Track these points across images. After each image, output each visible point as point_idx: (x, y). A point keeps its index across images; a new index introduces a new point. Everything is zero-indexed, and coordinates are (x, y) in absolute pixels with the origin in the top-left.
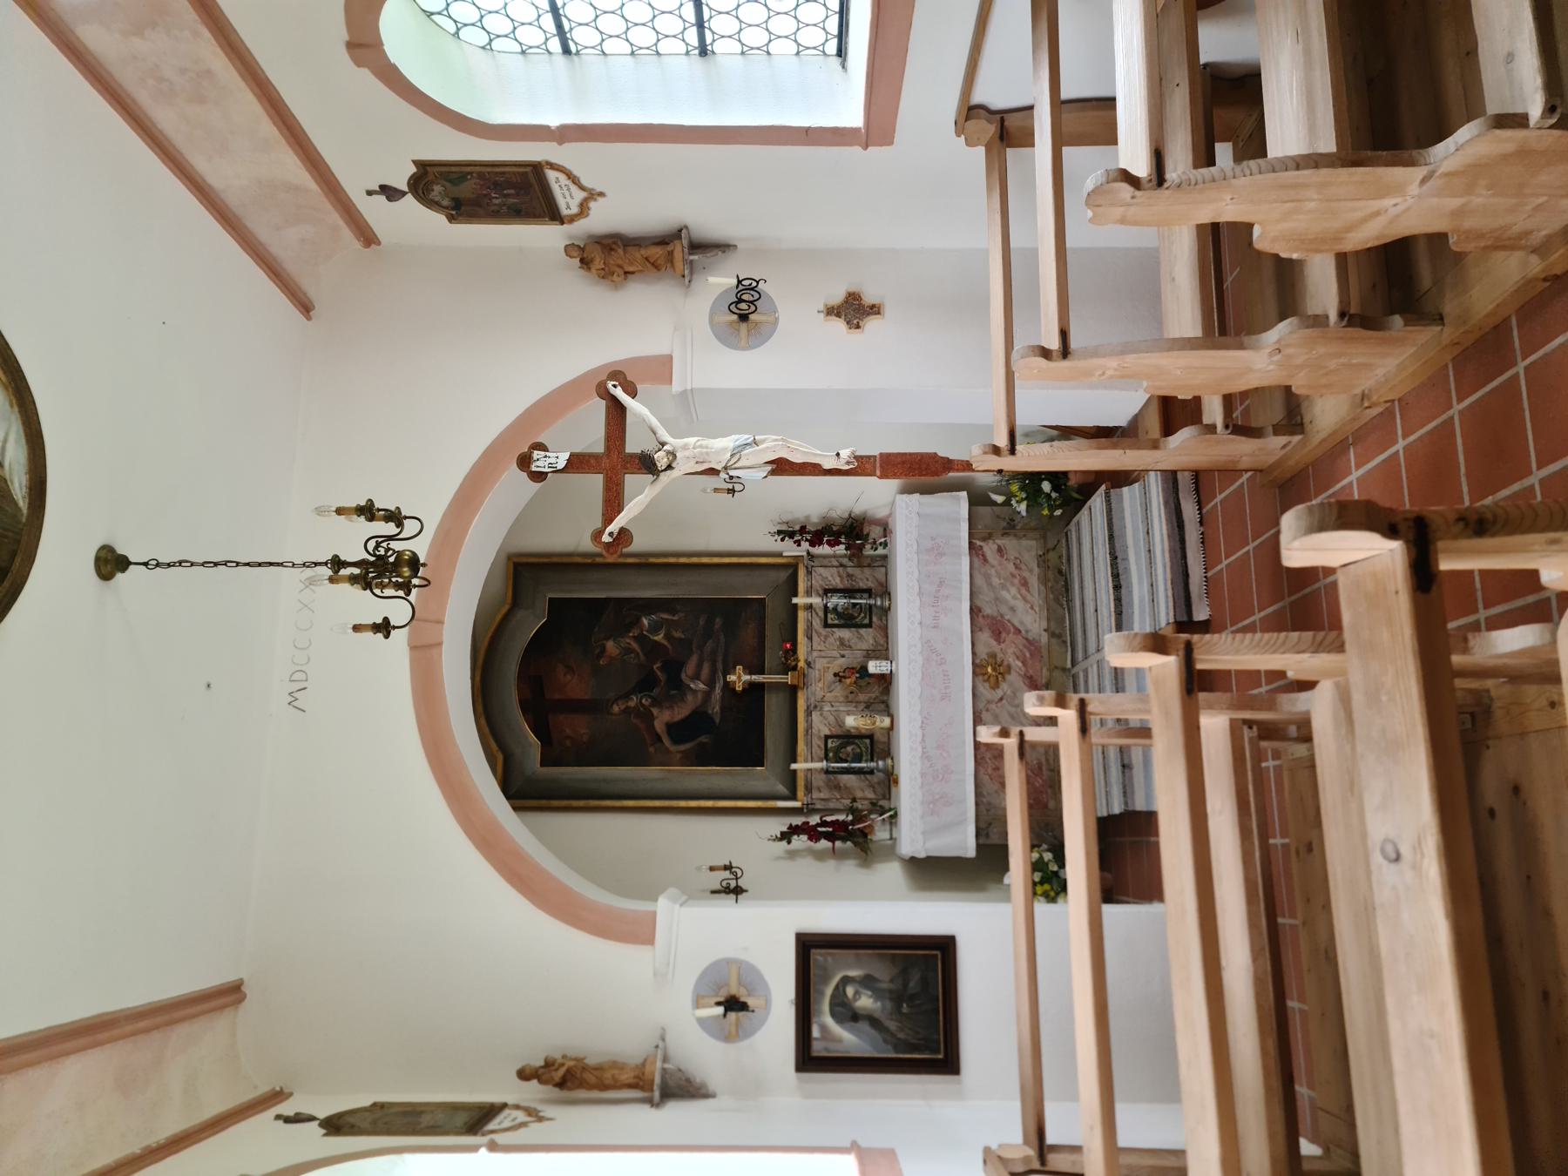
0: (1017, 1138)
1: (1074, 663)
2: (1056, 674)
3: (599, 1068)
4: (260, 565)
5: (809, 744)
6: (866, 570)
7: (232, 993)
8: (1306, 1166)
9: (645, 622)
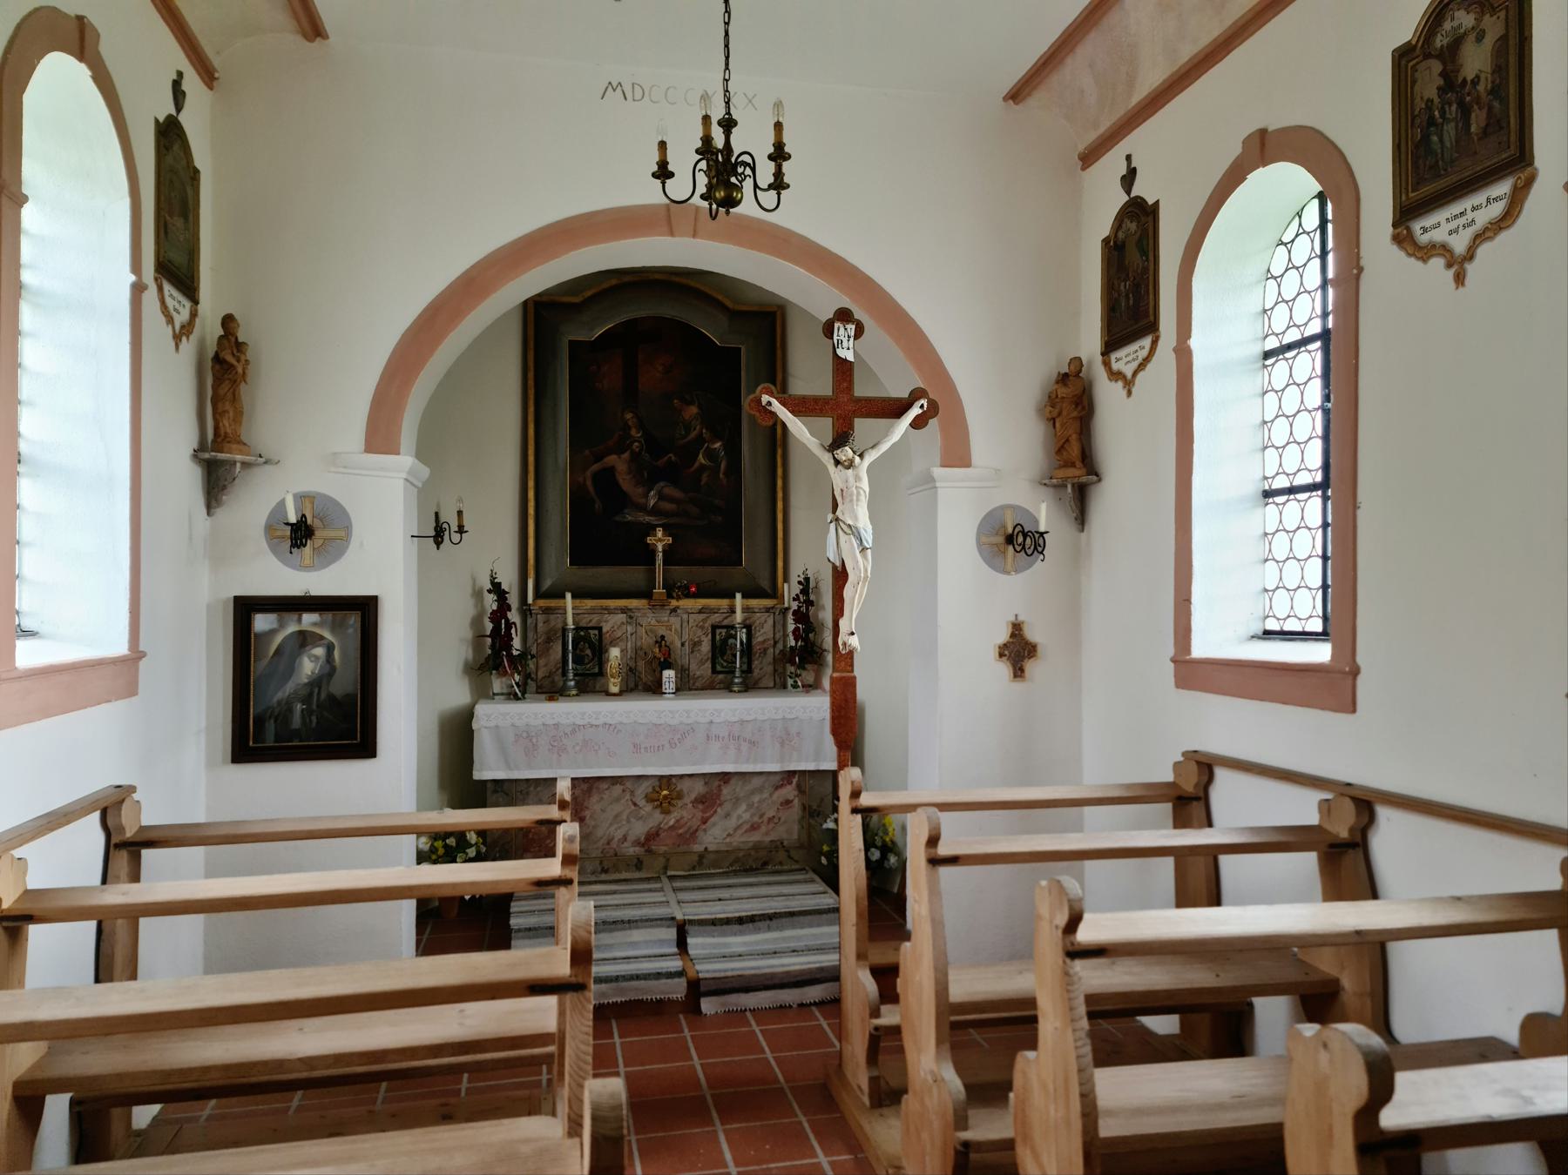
0: (147, 820)
1: (671, 878)
2: (662, 860)
3: (235, 399)
4: (727, 46)
5: (593, 611)
6: (770, 668)
7: (313, 29)
8: (116, 1112)
9: (717, 445)
